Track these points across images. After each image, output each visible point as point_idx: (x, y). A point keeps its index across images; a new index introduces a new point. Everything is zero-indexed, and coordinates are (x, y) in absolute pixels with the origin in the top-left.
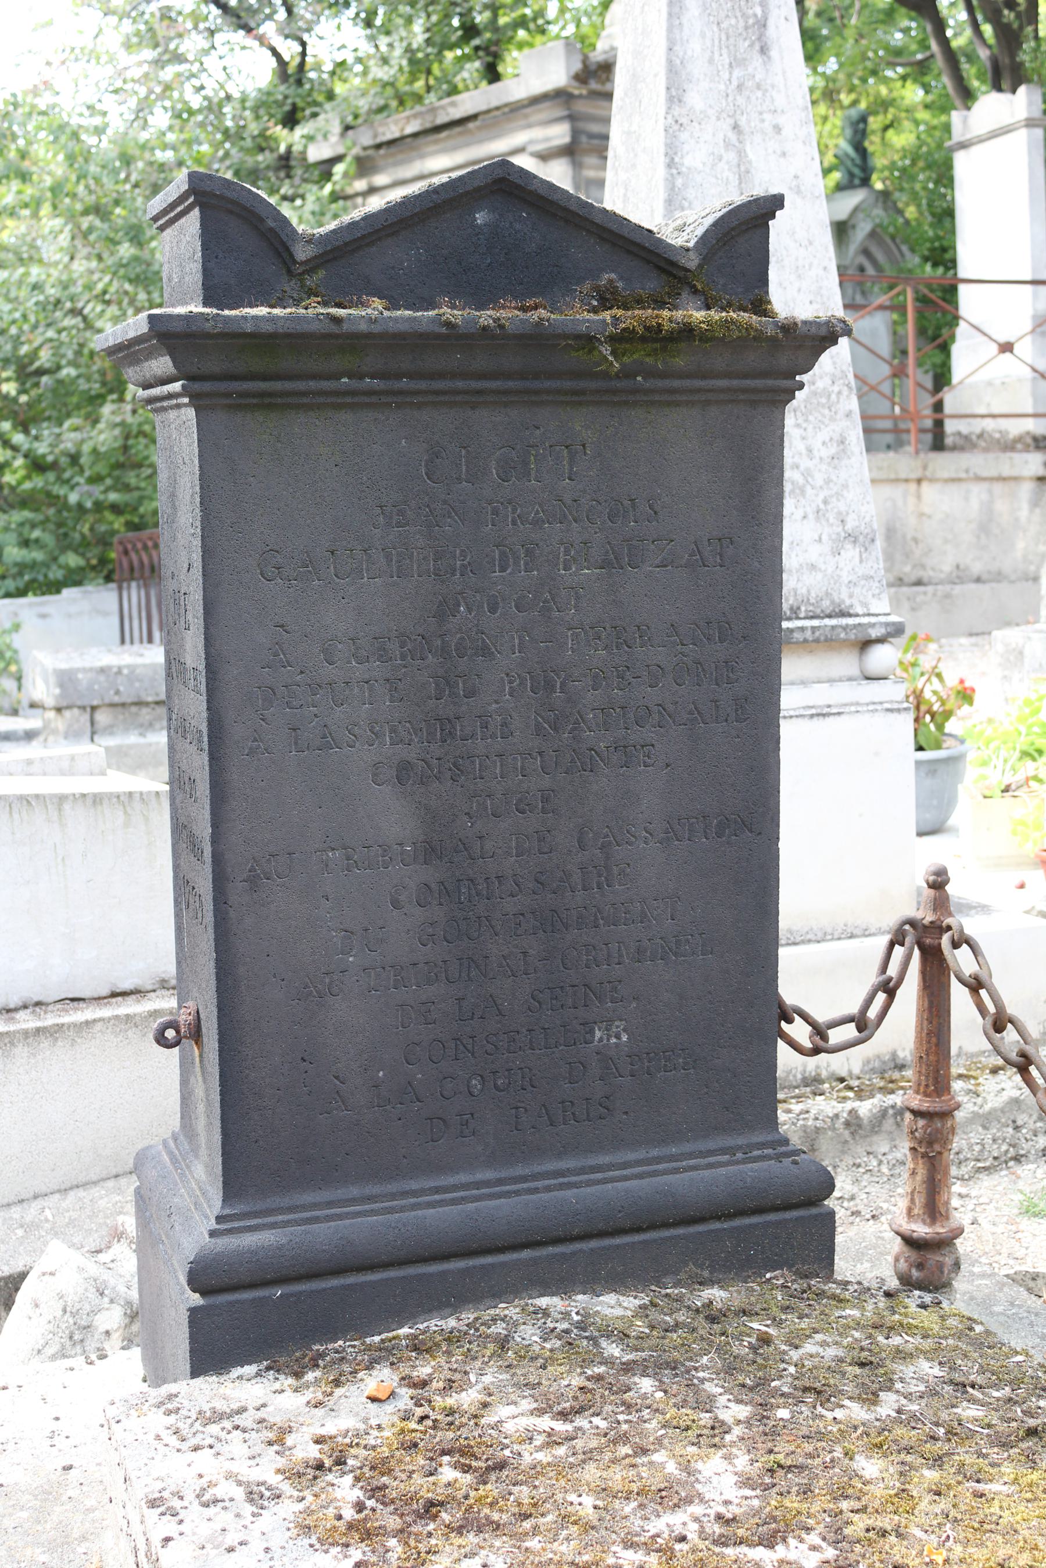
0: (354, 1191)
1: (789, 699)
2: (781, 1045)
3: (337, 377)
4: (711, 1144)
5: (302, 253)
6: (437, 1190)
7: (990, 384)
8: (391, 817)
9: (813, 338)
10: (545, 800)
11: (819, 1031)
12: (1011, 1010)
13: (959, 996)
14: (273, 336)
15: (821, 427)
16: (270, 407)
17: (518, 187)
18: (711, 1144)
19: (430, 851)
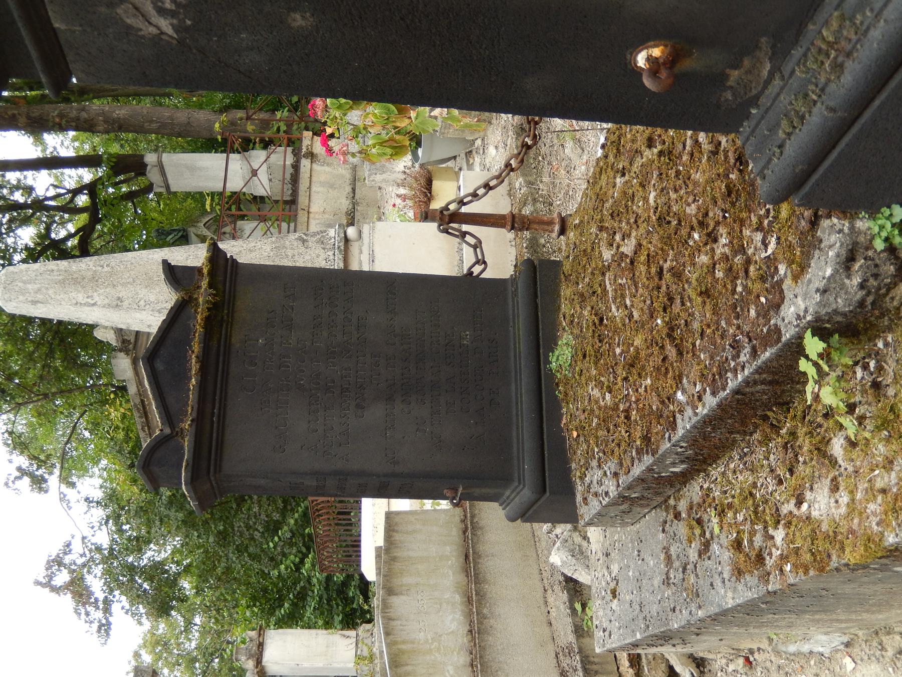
0: (514, 434)
1: (366, 268)
2: (482, 276)
3: (213, 421)
4: (511, 303)
5: (168, 431)
6: (517, 403)
7: (270, 180)
8: (376, 413)
9: (214, 250)
10: (375, 356)
11: (478, 262)
12: (472, 191)
13: (464, 210)
14: (195, 442)
15: (252, 248)
16: (222, 442)
17: (151, 354)
18: (511, 303)
19: (390, 399)
